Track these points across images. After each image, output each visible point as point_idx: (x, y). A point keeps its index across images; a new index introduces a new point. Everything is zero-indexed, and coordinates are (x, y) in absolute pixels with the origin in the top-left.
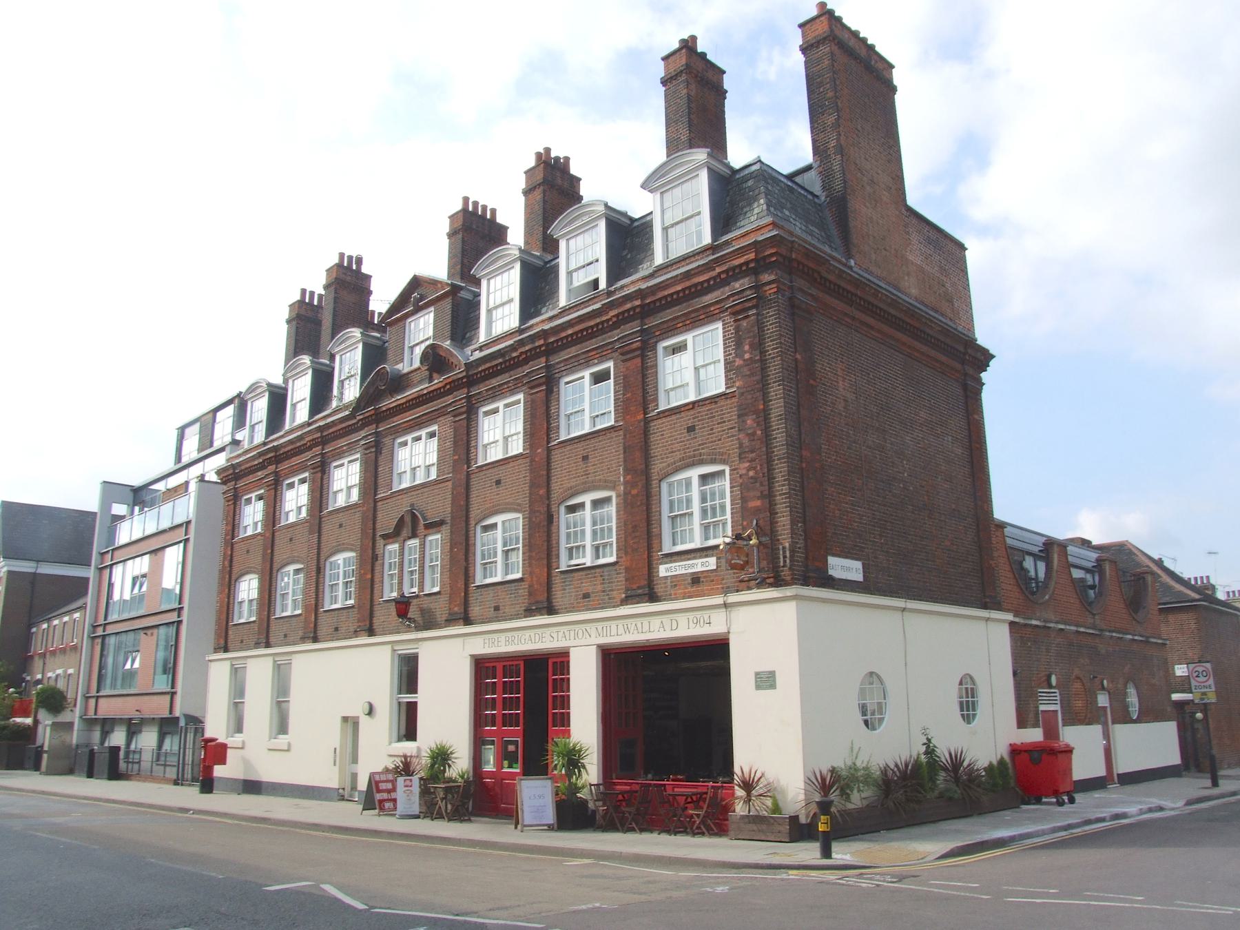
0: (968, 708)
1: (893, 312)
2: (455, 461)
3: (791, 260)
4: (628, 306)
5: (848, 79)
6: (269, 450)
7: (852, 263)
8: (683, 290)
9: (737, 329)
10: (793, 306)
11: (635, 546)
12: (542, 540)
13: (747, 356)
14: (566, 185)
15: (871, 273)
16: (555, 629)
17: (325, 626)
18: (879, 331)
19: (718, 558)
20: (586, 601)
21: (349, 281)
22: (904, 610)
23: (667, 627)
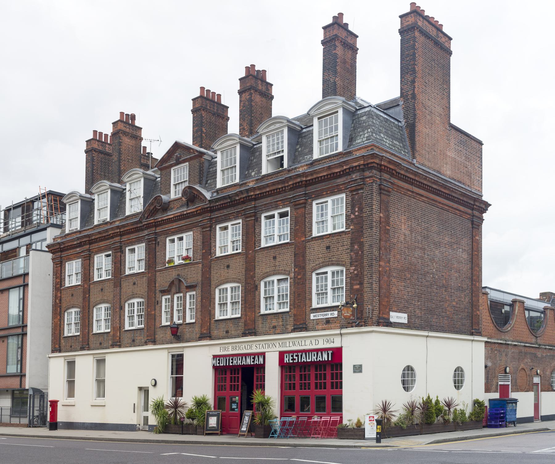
0: (458, 383)
1: (434, 186)
2: (203, 253)
3: (381, 165)
4: (299, 180)
5: (425, 46)
6: (85, 236)
7: (415, 161)
8: (327, 175)
9: (353, 199)
10: (380, 189)
11: (299, 304)
12: (250, 299)
13: (357, 214)
14: (264, 89)
15: (425, 166)
16: (258, 343)
17: (126, 339)
18: (426, 197)
19: (338, 312)
20: (274, 330)
21: (127, 127)
22: (427, 336)
23: (314, 343)
